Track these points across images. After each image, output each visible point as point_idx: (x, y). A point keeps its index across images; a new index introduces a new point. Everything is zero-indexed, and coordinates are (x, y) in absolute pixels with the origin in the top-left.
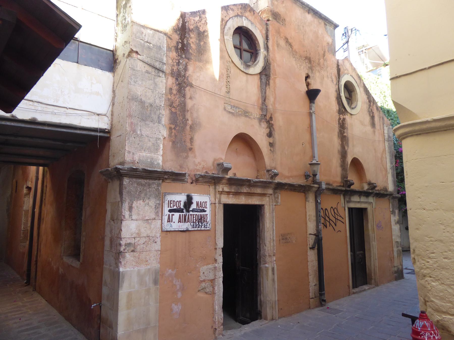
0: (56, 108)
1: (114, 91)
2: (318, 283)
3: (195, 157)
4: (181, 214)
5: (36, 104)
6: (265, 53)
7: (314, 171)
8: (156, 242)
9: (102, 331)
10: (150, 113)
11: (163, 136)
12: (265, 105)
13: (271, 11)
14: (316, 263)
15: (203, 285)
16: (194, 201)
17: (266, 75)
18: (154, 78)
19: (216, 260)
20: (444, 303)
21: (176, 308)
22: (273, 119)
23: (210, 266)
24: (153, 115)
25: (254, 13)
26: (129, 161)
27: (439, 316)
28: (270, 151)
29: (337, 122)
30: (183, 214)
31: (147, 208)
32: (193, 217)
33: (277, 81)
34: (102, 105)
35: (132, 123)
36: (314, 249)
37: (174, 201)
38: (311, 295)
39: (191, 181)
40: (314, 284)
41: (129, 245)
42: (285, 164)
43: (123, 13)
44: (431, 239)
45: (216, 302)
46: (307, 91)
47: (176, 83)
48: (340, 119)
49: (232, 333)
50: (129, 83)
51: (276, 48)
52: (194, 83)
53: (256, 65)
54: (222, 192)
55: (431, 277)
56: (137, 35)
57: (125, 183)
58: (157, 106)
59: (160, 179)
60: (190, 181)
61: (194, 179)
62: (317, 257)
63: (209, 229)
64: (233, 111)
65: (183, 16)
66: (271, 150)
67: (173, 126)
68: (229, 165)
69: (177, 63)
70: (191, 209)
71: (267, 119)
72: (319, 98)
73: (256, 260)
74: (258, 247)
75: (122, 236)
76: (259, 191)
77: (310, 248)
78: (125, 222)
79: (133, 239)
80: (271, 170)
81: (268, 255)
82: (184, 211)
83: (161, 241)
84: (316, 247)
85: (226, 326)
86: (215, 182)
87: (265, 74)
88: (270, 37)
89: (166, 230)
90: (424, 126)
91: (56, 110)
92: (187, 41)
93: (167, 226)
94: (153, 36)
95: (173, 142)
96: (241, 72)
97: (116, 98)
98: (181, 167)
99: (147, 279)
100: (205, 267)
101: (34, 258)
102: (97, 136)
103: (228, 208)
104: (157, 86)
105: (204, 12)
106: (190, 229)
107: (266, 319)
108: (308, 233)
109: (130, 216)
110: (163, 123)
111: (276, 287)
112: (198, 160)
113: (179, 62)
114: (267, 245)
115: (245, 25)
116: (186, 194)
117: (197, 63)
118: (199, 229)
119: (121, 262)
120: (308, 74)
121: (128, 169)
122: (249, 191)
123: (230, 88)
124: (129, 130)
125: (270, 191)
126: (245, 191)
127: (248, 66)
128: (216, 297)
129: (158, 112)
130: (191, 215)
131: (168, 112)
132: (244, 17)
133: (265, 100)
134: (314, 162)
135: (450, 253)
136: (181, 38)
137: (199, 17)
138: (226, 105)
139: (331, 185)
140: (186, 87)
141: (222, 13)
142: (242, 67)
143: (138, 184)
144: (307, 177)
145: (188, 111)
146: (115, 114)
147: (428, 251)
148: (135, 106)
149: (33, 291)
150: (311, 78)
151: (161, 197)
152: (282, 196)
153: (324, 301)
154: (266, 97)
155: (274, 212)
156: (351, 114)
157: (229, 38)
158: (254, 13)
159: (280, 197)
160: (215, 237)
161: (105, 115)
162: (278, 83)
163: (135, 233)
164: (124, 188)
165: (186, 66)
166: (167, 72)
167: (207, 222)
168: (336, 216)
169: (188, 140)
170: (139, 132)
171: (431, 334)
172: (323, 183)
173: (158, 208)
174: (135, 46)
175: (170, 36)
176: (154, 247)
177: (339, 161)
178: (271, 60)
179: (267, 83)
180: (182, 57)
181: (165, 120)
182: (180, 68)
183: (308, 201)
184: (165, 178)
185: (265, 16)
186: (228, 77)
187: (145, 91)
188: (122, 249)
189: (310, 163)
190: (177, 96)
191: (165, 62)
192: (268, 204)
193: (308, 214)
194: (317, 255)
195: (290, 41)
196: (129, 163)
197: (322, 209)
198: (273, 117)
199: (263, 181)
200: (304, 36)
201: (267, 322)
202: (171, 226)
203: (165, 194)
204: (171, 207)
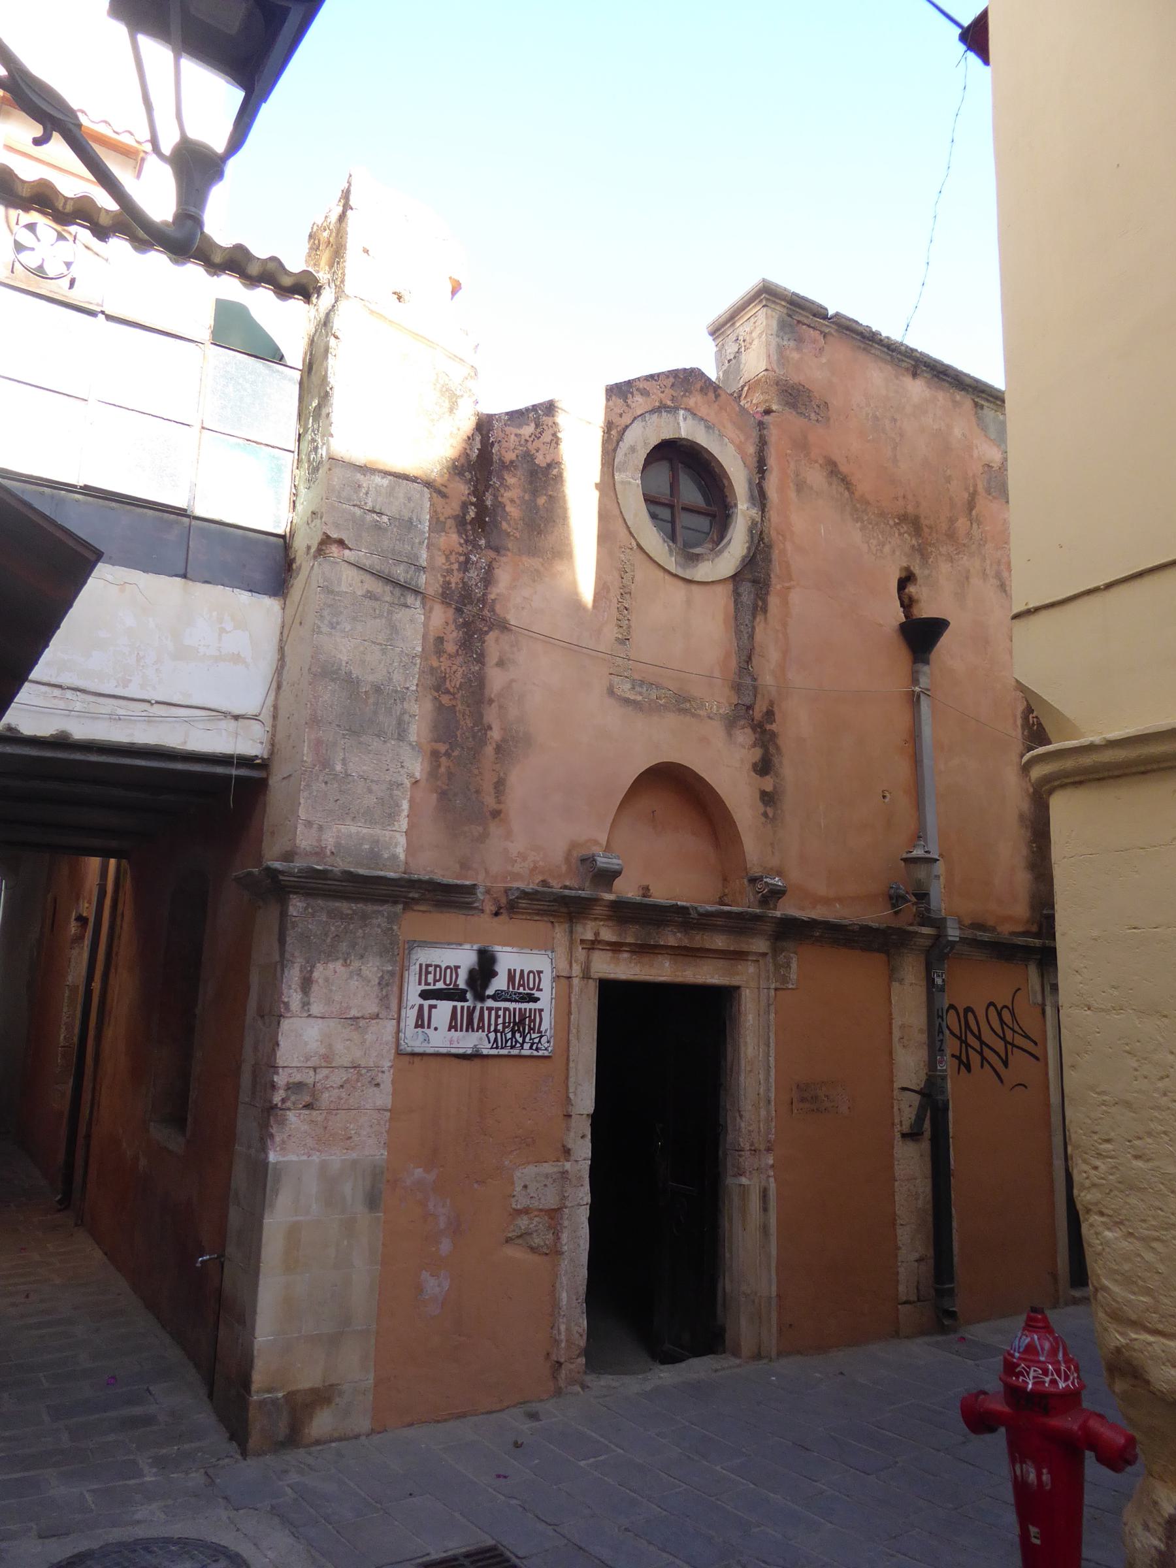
0: (121, 702)
1: (281, 650)
2: (931, 1253)
3: (508, 835)
4: (459, 1004)
5: (69, 694)
6: (754, 513)
7: (919, 883)
8: (378, 1085)
9: (221, 1333)
11: (410, 776)
13: (777, 384)
14: (924, 1188)
15: (523, 1222)
16: (502, 968)
17: (755, 582)
18: (390, 613)
19: (567, 1152)
20: (1134, 1293)
21: (434, 1285)
22: (778, 716)
23: (548, 1168)
25: (717, 396)
26: (308, 849)
27: (1121, 1334)
28: (763, 819)
29: (1019, 722)
30: (466, 1004)
31: (354, 983)
32: (497, 1017)
33: (795, 597)
34: (248, 691)
35: (319, 742)
36: (917, 1141)
37: (436, 966)
38: (904, 1290)
39: (494, 909)
40: (916, 1256)
41: (296, 1087)
42: (815, 857)
43: (313, 431)
44: (1105, 1098)
45: (564, 1279)
46: (902, 627)
47: (455, 621)
49: (614, 1384)
50: (316, 630)
51: (792, 494)
53: (721, 552)
54: (593, 942)
55: (1102, 1214)
56: (344, 494)
57: (292, 911)
58: (396, 691)
59: (395, 903)
60: (489, 907)
61: (504, 901)
62: (929, 1165)
63: (546, 1053)
64: (639, 698)
65: (484, 425)
66: (765, 815)
67: (442, 748)
68: (615, 861)
69: (460, 563)
70: (490, 991)
71: (757, 720)
72: (946, 641)
75: (280, 1062)
76: (719, 942)
78: (291, 1020)
79: (312, 1073)
80: (760, 879)
81: (747, 1147)
82: (469, 996)
83: (393, 1082)
84: (927, 1134)
85: (598, 1356)
86: (569, 913)
87: (755, 579)
88: (772, 461)
89: (409, 1050)
90: (1087, 760)
91: (122, 709)
92: (495, 497)
93: (413, 1040)
94: (391, 492)
95: (443, 795)
96: (667, 577)
97: (286, 668)
98: (465, 865)
99: (347, 1189)
100: (531, 1170)
101: (82, 1130)
102: (229, 777)
103: (612, 995)
104: (397, 633)
105: (549, 408)
106: (485, 1052)
107: (736, 1353)
108: (897, 1085)
109: (305, 1004)
111: (774, 1252)
112: (516, 847)
113: (468, 560)
114: (746, 1115)
115: (684, 435)
116: (475, 947)
117: (524, 558)
118: (515, 1052)
119: (272, 1136)
120: (907, 569)
121: (300, 871)
122: (686, 942)
123: (629, 627)
124: (309, 760)
125: (760, 945)
126: (672, 941)
127: (693, 559)
128: (565, 1264)
129: (399, 708)
130: (490, 1009)
131: (428, 705)
132: (682, 412)
133: (749, 660)
134: (918, 852)
135: (1149, 1140)
136: (475, 493)
137: (533, 425)
138: (616, 679)
139: (993, 929)
140: (487, 633)
141: (607, 407)
142: (671, 564)
143: (332, 914)
144: (895, 900)
145: (491, 701)
146: (283, 714)
147: (1095, 1133)
148: (329, 695)
149: (76, 1225)
150: (919, 581)
151: (397, 953)
152: (800, 963)
153: (952, 1315)
154: (752, 649)
155: (772, 1008)
157: (631, 481)
158: (717, 396)
159: (794, 965)
160: (567, 1078)
161: (255, 718)
162: (799, 604)
163: (316, 1053)
164: (289, 925)
165: (490, 569)
166: (431, 591)
167: (539, 1032)
168: (1009, 1033)
169: (488, 787)
170: (339, 767)
171: (1045, 1372)
172: (949, 923)
173: (387, 985)
174: (337, 526)
175: (443, 489)
176: (381, 1098)
177: (1024, 851)
178: (773, 534)
179: (760, 606)
180: (476, 546)
181: (418, 729)
182: (470, 578)
183: (901, 981)
184: (413, 899)
185: (755, 401)
186: (625, 593)
187: (362, 649)
188: (277, 1099)
189: (905, 856)
190: (460, 660)
191: (424, 564)
192: (753, 984)
193: (897, 1022)
194: (928, 1159)
195: (844, 468)
196: (307, 854)
197: (952, 1007)
198: (776, 709)
199: (729, 912)
200: (894, 449)
201: (738, 1361)
202: (427, 1040)
203: (412, 945)
204: (427, 984)
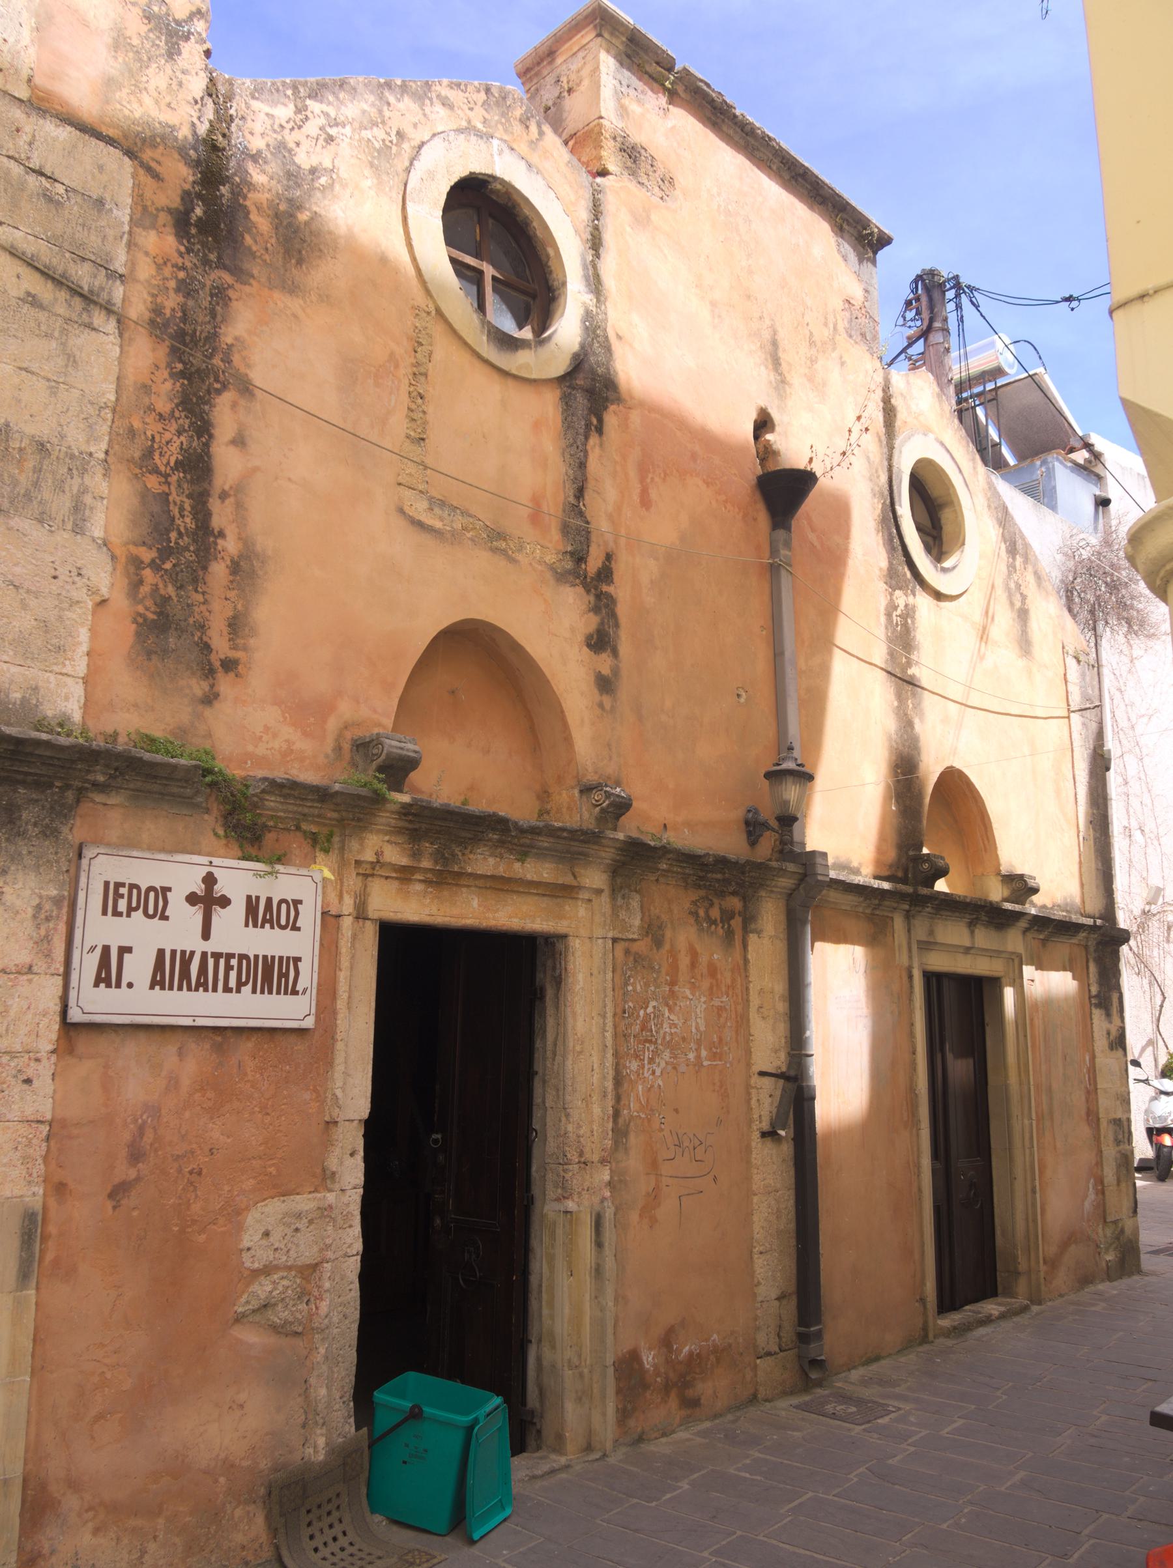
6: (589, 299)
8: (28, 1081)
10: (36, 484)
11: (92, 591)
12: (581, 514)
18: (64, 331)
24: (46, 494)
32: (229, 968)
37: (132, 886)
40: (774, 1293)
48: (892, 607)
52: (257, 376)
58: (72, 457)
66: (601, 706)
67: (147, 555)
68: (410, 746)
71: (590, 574)
73: (528, 1128)
74: (536, 1125)
77: (764, 1135)
88: (608, 237)
93: (95, 1003)
96: (478, 365)
110: (98, 533)
117: (277, 295)
122: (501, 870)
123: (425, 423)
138: (408, 493)
156: (938, 596)
173: (48, 919)
183: (759, 932)
184: (95, 785)
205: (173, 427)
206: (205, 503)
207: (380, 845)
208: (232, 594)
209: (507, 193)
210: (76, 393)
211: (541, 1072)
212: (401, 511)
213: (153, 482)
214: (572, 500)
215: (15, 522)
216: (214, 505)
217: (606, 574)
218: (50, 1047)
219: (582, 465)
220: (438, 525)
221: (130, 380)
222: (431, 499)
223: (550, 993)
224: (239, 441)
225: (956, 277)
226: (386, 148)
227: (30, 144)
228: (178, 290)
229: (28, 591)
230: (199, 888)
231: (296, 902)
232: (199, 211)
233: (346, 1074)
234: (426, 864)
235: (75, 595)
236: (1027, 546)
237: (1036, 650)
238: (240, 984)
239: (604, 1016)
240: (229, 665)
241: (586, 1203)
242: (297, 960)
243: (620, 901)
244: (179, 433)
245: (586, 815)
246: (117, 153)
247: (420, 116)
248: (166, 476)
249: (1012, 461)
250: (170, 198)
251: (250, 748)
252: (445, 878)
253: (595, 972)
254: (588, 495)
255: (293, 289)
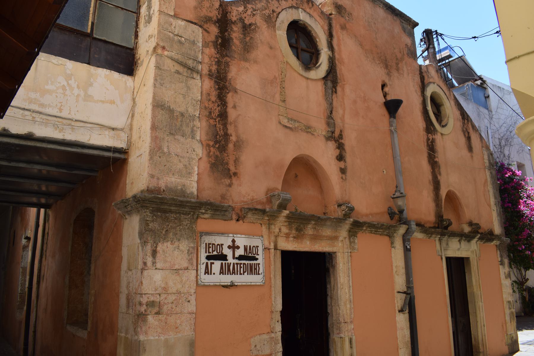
8: (189, 301)
10: (181, 125)
12: (332, 118)
18: (186, 80)
24: (184, 128)
32: (241, 267)
37: (213, 244)
48: (428, 139)
52: (238, 87)
58: (190, 116)
66: (342, 178)
68: (288, 196)
71: (336, 138)
88: (334, 33)
173: (191, 253)
205: (216, 105)
206: (226, 126)
207: (281, 224)
208: (235, 153)
209: (304, 24)
210: (190, 98)
211: (329, 294)
212: (280, 123)
213: (212, 121)
214: (329, 114)
215: (176, 137)
216: (229, 127)
217: (341, 136)
218: (194, 291)
219: (331, 104)
220: (291, 126)
221: (204, 92)
222: (288, 119)
223: (331, 270)
224: (234, 107)
225: (436, 31)
226: (269, 16)
227: (175, 27)
228: (215, 65)
229: (181, 157)
230: (230, 244)
231: (257, 247)
232: (220, 41)
233: (275, 298)
234: (294, 232)
235: (193, 157)
236: (468, 116)
237: (474, 149)
238: (244, 272)
239: (349, 277)
240: (235, 174)
241: (346, 335)
242: (257, 247)
243: (352, 240)
244: (218, 106)
245: (340, 214)
246: (197, 27)
247: (278, 5)
248: (215, 119)
249: (456, 85)
250: (212, 38)
251: (242, 199)
252: (299, 236)
253: (345, 263)
254: (333, 112)
255: (246, 60)
